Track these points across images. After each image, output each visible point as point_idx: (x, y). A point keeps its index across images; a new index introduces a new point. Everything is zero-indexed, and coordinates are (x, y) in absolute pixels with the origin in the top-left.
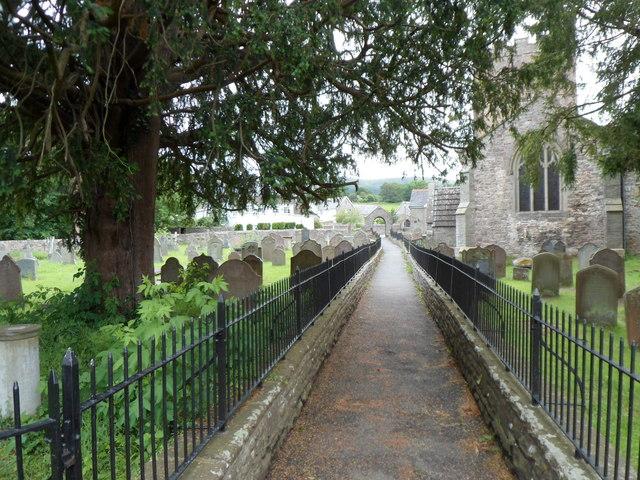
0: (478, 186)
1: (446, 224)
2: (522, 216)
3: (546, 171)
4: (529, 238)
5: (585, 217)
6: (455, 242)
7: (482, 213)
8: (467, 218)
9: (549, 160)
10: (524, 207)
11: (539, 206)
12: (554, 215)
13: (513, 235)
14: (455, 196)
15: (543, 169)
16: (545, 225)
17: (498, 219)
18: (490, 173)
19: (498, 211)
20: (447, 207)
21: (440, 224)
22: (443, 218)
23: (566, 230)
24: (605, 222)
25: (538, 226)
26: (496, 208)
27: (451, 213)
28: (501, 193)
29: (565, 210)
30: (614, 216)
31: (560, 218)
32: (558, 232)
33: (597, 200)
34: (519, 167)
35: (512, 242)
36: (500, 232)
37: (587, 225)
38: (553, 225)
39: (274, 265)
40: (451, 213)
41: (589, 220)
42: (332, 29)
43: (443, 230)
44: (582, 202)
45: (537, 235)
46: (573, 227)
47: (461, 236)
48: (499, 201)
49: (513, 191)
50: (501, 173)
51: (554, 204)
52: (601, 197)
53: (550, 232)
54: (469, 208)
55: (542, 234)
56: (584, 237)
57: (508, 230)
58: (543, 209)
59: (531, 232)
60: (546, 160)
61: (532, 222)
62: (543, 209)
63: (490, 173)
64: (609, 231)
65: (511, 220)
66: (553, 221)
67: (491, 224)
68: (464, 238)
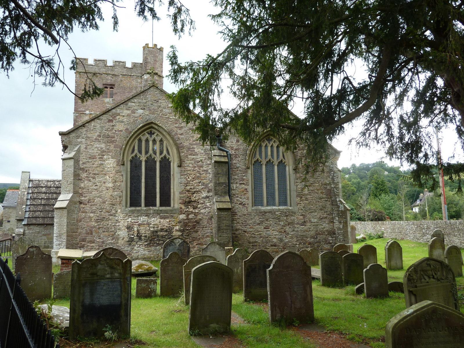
0: (84, 175)
1: (41, 221)
2: (133, 212)
3: (143, 164)
4: (139, 237)
5: (196, 214)
6: (52, 242)
7: (87, 208)
8: (68, 213)
9: (147, 152)
10: (134, 202)
11: (150, 202)
12: (166, 212)
13: (123, 233)
14: (53, 190)
15: (141, 161)
16: (157, 222)
17: (104, 214)
18: (98, 162)
19: (107, 206)
20: (43, 202)
21: (34, 221)
22: (37, 214)
23: (177, 228)
24: (214, 221)
25: (149, 224)
26: (104, 202)
27: (47, 208)
28: (111, 185)
29: (177, 206)
30: (224, 214)
31: (171, 214)
32: (169, 231)
33: (207, 197)
34: (130, 158)
35: (121, 242)
36: (107, 230)
37: (198, 222)
38: (165, 223)
39: (276, 321)
40: (47, 208)
41: (199, 217)
42: (198, 98)
43: (37, 229)
44: (193, 199)
45: (148, 234)
46: (185, 224)
47: (60, 236)
48: (107, 195)
49: (124, 183)
50: (110, 163)
51: (166, 201)
52: (211, 194)
53: (162, 230)
54: (71, 201)
55: (153, 232)
56: (194, 235)
57: (117, 228)
58: (155, 205)
59: (143, 230)
60: (158, 154)
61: (142, 219)
62: (155, 205)
63: (98, 162)
64: (219, 229)
65: (120, 216)
66: (164, 218)
67: (97, 221)
68: (64, 237)
